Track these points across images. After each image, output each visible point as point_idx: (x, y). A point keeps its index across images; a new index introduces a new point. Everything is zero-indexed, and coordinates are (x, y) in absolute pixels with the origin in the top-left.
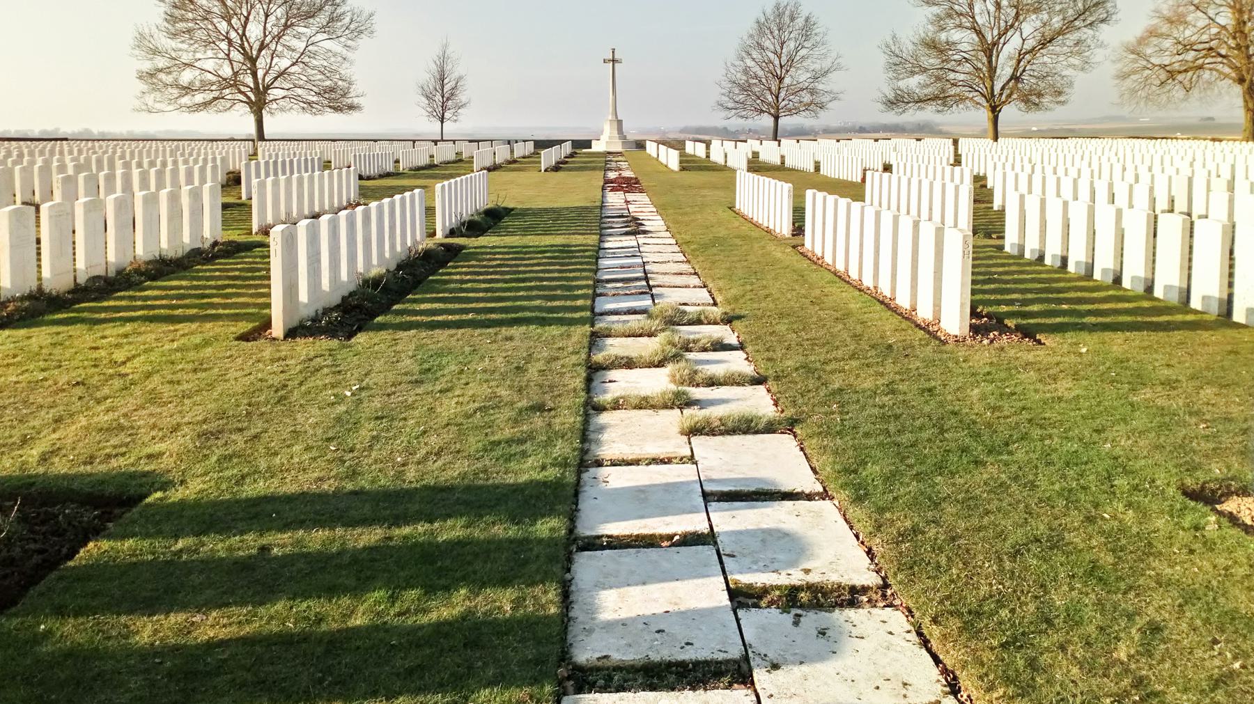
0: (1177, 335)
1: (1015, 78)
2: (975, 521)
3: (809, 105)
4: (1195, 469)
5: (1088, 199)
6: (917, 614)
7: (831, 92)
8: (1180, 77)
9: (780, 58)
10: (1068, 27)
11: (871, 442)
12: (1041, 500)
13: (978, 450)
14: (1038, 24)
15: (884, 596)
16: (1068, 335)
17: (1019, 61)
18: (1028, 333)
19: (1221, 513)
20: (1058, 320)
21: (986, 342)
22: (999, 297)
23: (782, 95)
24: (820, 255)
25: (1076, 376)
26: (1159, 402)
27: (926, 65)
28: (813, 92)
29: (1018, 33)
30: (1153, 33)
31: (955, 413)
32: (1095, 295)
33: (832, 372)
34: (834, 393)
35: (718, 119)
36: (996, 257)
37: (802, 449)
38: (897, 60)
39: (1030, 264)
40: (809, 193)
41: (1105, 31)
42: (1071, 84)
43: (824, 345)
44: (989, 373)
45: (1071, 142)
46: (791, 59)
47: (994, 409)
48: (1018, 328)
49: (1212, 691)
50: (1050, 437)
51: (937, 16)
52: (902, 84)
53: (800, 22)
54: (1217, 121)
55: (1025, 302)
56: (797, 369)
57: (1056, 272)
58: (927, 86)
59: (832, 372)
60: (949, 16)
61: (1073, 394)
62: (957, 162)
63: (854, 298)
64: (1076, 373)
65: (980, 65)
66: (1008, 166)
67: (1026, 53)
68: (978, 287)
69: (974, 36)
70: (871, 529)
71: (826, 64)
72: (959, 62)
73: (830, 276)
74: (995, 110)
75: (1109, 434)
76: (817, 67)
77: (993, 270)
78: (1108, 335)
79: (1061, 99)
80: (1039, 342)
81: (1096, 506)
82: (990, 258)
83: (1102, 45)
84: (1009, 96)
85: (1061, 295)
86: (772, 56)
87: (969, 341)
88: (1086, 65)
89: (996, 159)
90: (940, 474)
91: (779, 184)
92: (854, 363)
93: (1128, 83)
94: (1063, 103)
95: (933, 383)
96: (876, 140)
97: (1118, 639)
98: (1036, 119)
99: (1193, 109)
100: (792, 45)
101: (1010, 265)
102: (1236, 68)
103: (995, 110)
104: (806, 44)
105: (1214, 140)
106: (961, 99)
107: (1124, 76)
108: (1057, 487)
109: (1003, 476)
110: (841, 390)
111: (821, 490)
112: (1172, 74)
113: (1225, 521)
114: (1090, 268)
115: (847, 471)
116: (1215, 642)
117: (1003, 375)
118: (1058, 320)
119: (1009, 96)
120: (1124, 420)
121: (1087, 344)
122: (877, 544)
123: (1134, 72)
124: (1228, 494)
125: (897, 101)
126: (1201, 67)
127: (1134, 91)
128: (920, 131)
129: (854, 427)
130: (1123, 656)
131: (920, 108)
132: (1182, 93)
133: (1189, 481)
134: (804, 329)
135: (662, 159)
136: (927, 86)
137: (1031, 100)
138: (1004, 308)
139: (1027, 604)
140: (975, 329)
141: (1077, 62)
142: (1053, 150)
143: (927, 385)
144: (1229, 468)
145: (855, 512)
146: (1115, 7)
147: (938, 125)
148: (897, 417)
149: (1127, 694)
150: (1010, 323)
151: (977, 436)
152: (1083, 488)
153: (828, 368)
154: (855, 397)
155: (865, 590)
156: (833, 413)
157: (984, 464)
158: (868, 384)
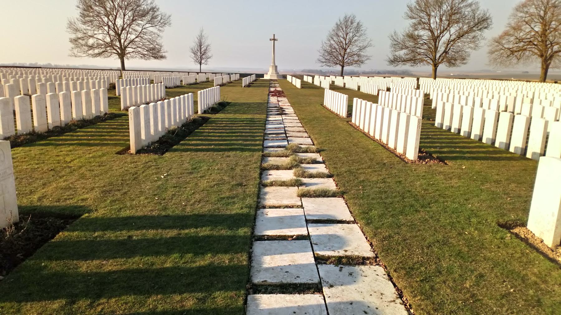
0: (503, 162)
1: (446, 52)
2: (414, 234)
4: (504, 216)
6: (388, 268)
8: (516, 54)
9: (345, 40)
10: (470, 30)
11: (375, 202)
13: (417, 206)
14: (458, 28)
15: (376, 261)
16: (458, 161)
17: (448, 45)
18: (441, 160)
19: (512, 233)
20: (454, 155)
21: (424, 163)
22: (431, 145)
23: (346, 57)
24: (358, 125)
25: (459, 178)
26: (492, 189)
27: (408, 45)
28: (359, 56)
29: (448, 32)
30: (506, 34)
32: (471, 145)
33: (361, 173)
34: (360, 182)
36: (431, 128)
37: (346, 204)
38: (395, 43)
39: (445, 131)
40: (355, 99)
42: (469, 56)
44: (424, 176)
46: (350, 41)
47: (425, 190)
48: (438, 158)
49: (501, 299)
50: (447, 202)
51: (414, 24)
53: (355, 24)
55: (442, 147)
56: (346, 172)
57: (455, 135)
58: (407, 54)
59: (361, 173)
60: (420, 24)
61: (458, 185)
62: (418, 88)
63: (371, 143)
65: (431, 46)
66: (439, 90)
69: (430, 33)
71: (365, 44)
72: (422, 44)
74: (436, 66)
75: (471, 201)
76: (361, 45)
77: (430, 133)
79: (464, 62)
80: (446, 164)
81: (463, 229)
82: (429, 129)
83: (484, 39)
84: (442, 60)
87: (417, 162)
88: (476, 48)
91: (343, 95)
92: (370, 170)
93: (494, 56)
94: (465, 63)
96: (384, 78)
97: (466, 279)
98: (453, 70)
99: (520, 68)
100: (351, 35)
101: (436, 132)
102: (540, 50)
103: (436, 66)
104: (357, 35)
105: (527, 81)
106: (422, 61)
107: (492, 52)
108: (448, 221)
110: (363, 181)
112: (512, 52)
113: (513, 236)
114: (470, 133)
115: (364, 213)
116: (504, 281)
117: (430, 176)
118: (454, 155)
119: (442, 60)
120: (477, 196)
121: (465, 165)
123: (497, 51)
124: (516, 226)
125: (394, 61)
127: (495, 59)
128: (403, 74)
130: (468, 286)
133: (501, 220)
135: (294, 83)
136: (407, 54)
137: (451, 62)
138: (433, 150)
140: (420, 158)
142: (459, 84)
143: (399, 180)
144: (517, 216)
145: (366, 229)
146: (491, 22)
148: (386, 192)
150: (435, 156)
151: (417, 200)
152: (458, 222)
153: (359, 172)
154: (369, 184)
155: (368, 258)
156: (360, 190)
157: (419, 211)
158: (375, 179)
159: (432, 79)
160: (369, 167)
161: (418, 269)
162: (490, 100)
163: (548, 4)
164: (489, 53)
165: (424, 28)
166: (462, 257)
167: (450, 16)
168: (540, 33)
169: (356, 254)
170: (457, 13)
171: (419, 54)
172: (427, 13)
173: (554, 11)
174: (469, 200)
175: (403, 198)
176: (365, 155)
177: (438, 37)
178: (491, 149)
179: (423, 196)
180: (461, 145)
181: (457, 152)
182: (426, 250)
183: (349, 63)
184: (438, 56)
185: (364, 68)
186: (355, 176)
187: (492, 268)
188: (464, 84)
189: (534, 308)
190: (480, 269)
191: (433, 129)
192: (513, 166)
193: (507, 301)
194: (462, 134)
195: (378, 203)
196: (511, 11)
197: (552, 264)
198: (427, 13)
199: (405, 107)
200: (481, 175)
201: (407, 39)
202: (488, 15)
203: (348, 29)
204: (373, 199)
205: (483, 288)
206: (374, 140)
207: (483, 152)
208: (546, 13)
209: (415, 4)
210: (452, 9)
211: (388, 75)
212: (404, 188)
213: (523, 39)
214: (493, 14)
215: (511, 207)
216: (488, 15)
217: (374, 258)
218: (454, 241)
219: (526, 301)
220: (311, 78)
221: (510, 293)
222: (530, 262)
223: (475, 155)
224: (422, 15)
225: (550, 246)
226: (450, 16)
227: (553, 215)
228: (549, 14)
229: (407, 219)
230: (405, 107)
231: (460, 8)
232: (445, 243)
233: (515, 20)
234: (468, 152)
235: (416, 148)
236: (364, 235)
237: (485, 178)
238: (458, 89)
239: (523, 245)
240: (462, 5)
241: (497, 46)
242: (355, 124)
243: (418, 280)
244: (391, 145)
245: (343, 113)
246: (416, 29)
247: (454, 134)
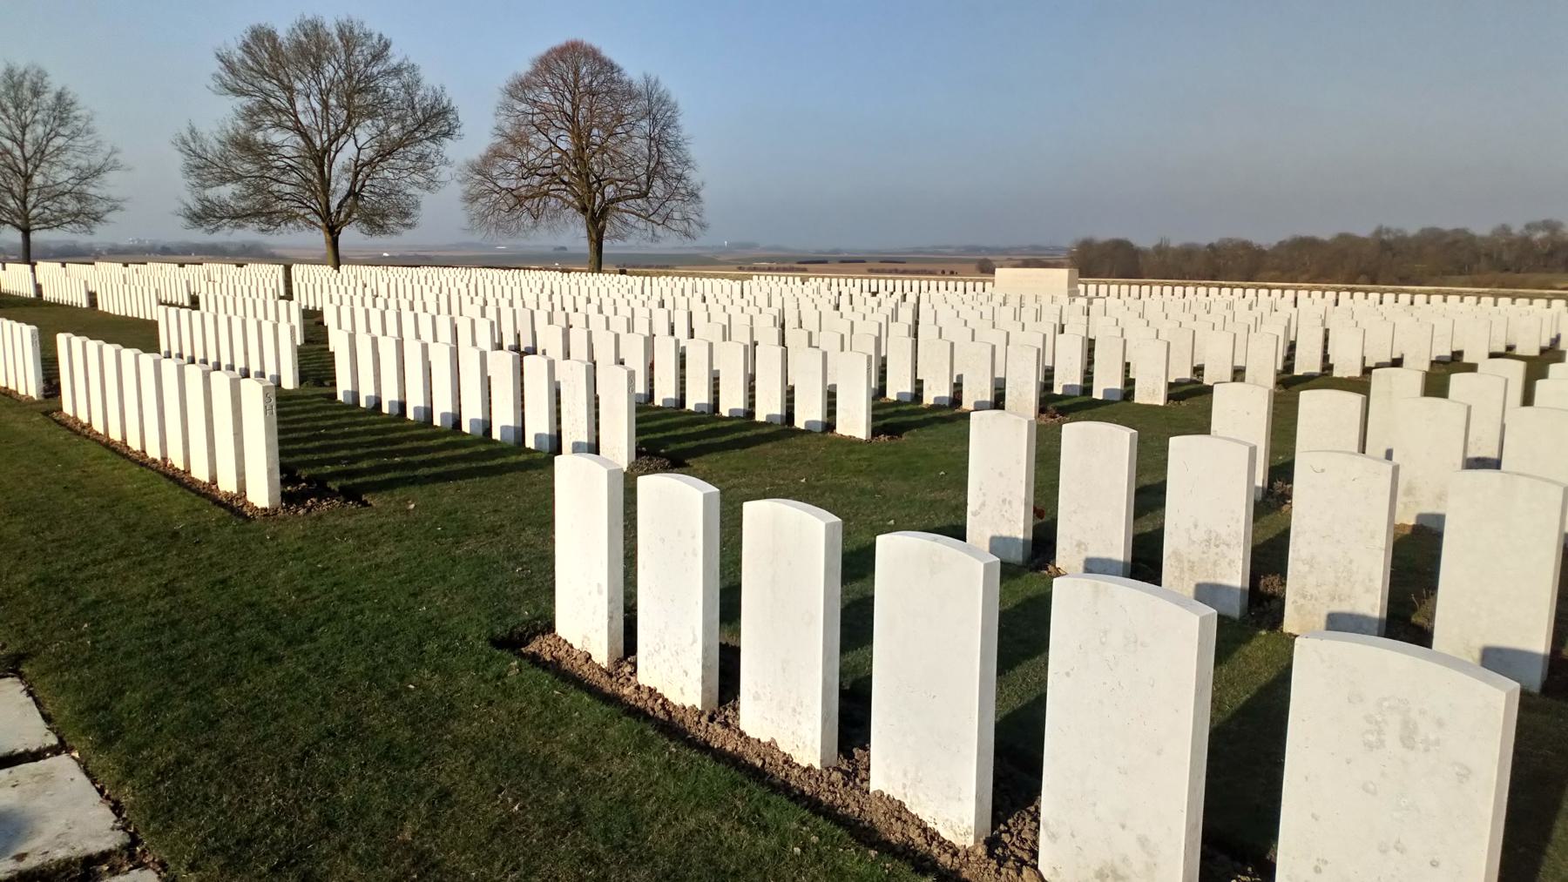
0: (509, 478)
1: (353, 193)
2: (260, 732)
3: (77, 215)
4: (505, 616)
5: (449, 340)
6: (172, 866)
7: (108, 199)
8: (527, 204)
9: (22, 147)
10: (408, 139)
11: (134, 663)
12: (341, 687)
13: (275, 644)
14: (374, 131)
15: (132, 857)
16: (397, 492)
17: (356, 174)
18: (352, 494)
19: (523, 656)
20: (388, 476)
21: (301, 512)
22: (324, 456)
23: (32, 199)
24: (85, 421)
25: (399, 537)
26: (481, 552)
27: (240, 171)
28: (80, 197)
29: (352, 141)
30: (496, 153)
31: (251, 605)
32: (431, 443)
33: (88, 580)
34: (87, 607)
36: (325, 408)
37: (30, 694)
38: (197, 161)
39: (365, 412)
40: (61, 338)
41: (449, 147)
42: (417, 205)
43: (79, 545)
44: (300, 549)
45: (422, 272)
46: (40, 151)
47: (300, 591)
48: (343, 490)
49: (490, 842)
50: (362, 612)
51: (249, 109)
52: (211, 193)
53: (48, 98)
54: (570, 251)
55: (353, 460)
56: (31, 585)
57: (393, 421)
58: (244, 198)
59: (88, 580)
60: (265, 111)
61: (393, 558)
62: (289, 296)
63: (131, 476)
64: (400, 534)
65: (309, 176)
66: (357, 301)
67: (363, 165)
69: (299, 139)
70: (118, 777)
71: (97, 160)
72: (283, 171)
73: (96, 450)
74: (333, 231)
75: (425, 597)
76: (83, 163)
77: (321, 423)
78: (438, 487)
79: (407, 221)
80: (365, 504)
81: (402, 678)
82: (318, 409)
83: (446, 163)
84: (349, 215)
86: (8, 144)
87: (281, 513)
88: (431, 185)
89: (342, 291)
90: (223, 684)
91: (17, 326)
92: (122, 563)
93: (477, 206)
94: (410, 226)
95: (228, 572)
96: (182, 265)
97: (404, 819)
98: (383, 243)
99: (542, 239)
100: (40, 130)
101: (340, 416)
102: (576, 196)
103: (333, 231)
104: (61, 130)
105: (563, 271)
106: (290, 217)
107: (472, 199)
108: (361, 668)
109: (301, 669)
110: (97, 602)
111: (54, 741)
112: (520, 200)
113: (526, 663)
114: (429, 412)
115: (93, 709)
116: (500, 790)
117: (316, 549)
118: (388, 476)
119: (349, 215)
120: (444, 578)
121: (413, 501)
122: (126, 799)
123: (482, 195)
124: (533, 636)
125: (205, 215)
126: (546, 194)
127: (484, 216)
128: (242, 256)
129: (112, 649)
130: (408, 836)
131: (241, 226)
132: (529, 221)
133: (498, 630)
134: (49, 528)
136: (244, 198)
137: (375, 221)
138: (329, 469)
139: (308, 812)
140: (287, 498)
141: (421, 180)
142: (488, 283)
143: (220, 576)
144: (537, 608)
145: (99, 761)
146: (457, 119)
147: (270, 247)
148: (174, 624)
149: (407, 874)
150: (333, 485)
151: (274, 628)
152: (390, 662)
153: (81, 576)
154: (115, 608)
155: (104, 856)
156: (82, 635)
157: (279, 660)
158: (139, 587)
159: (329, 268)
160: (121, 554)
161: (266, 837)
162: (434, 318)
163: (576, 86)
164: (466, 199)
165: (279, 125)
166: (395, 759)
167: (350, 97)
168: (571, 154)
169: (61, 854)
170: (366, 90)
171: (279, 198)
172: (280, 81)
173: (591, 104)
174: (421, 592)
175: (233, 630)
176: (106, 516)
177: (326, 151)
178: (482, 448)
179: (292, 612)
180: (408, 445)
181: (396, 467)
182: (292, 772)
183: (46, 221)
184: (334, 204)
185: (101, 235)
186: (67, 590)
187: (472, 763)
188: (503, 282)
189: (565, 834)
190: (443, 778)
191: (330, 409)
192: (533, 484)
193: (504, 840)
194: (410, 415)
195: (148, 663)
196: (498, 97)
197: (606, 709)
198: (280, 81)
199: (246, 353)
200: (454, 520)
201: (233, 152)
202: (445, 102)
204: (129, 655)
205: (448, 826)
206: (142, 464)
207: (463, 458)
208: (576, 108)
209: (239, 53)
210: (349, 77)
211: (197, 258)
212: (236, 598)
213: (537, 169)
214: (455, 96)
215: (523, 588)
216: (445, 102)
217: (124, 847)
218: (374, 721)
219: (546, 823)
221: (512, 817)
222: (562, 719)
223: (442, 469)
224: (267, 85)
225: (605, 665)
226: (350, 97)
227: (600, 592)
228: (583, 111)
229: (239, 693)
230: (246, 353)
231: (371, 78)
232: (353, 731)
233: (512, 120)
234: (423, 464)
235: (270, 472)
236: (94, 782)
237: (465, 527)
238: (409, 297)
239: (547, 679)
240: (375, 70)
241: (481, 183)
242: (75, 417)
243: (264, 869)
244: (200, 473)
245: (29, 385)
246: (257, 127)
247: (389, 418)
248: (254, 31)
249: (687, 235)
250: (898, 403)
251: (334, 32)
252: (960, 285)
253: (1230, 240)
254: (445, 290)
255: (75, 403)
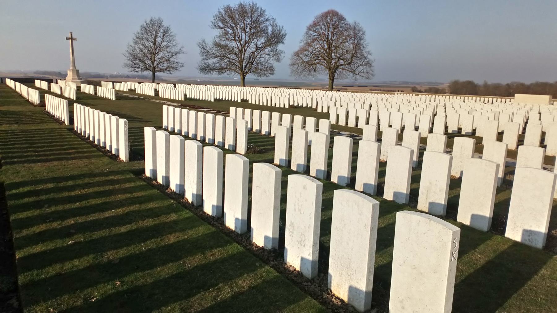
30: (302, 50)
35: (126, 71)
45: (209, 87)
52: (206, 62)
68: (270, 143)
85: (144, 206)
96: (140, 83)
107: (292, 65)
125: (206, 69)
135: (18, 90)
184: (244, 65)
196: (305, 30)
203: (155, 31)
220: (46, 83)
248: (241, 4)
249: (368, 78)
250: (254, 133)
251: (248, 5)
252: (462, 98)
253: (515, 83)
254: (258, 94)
255: (79, 125)
